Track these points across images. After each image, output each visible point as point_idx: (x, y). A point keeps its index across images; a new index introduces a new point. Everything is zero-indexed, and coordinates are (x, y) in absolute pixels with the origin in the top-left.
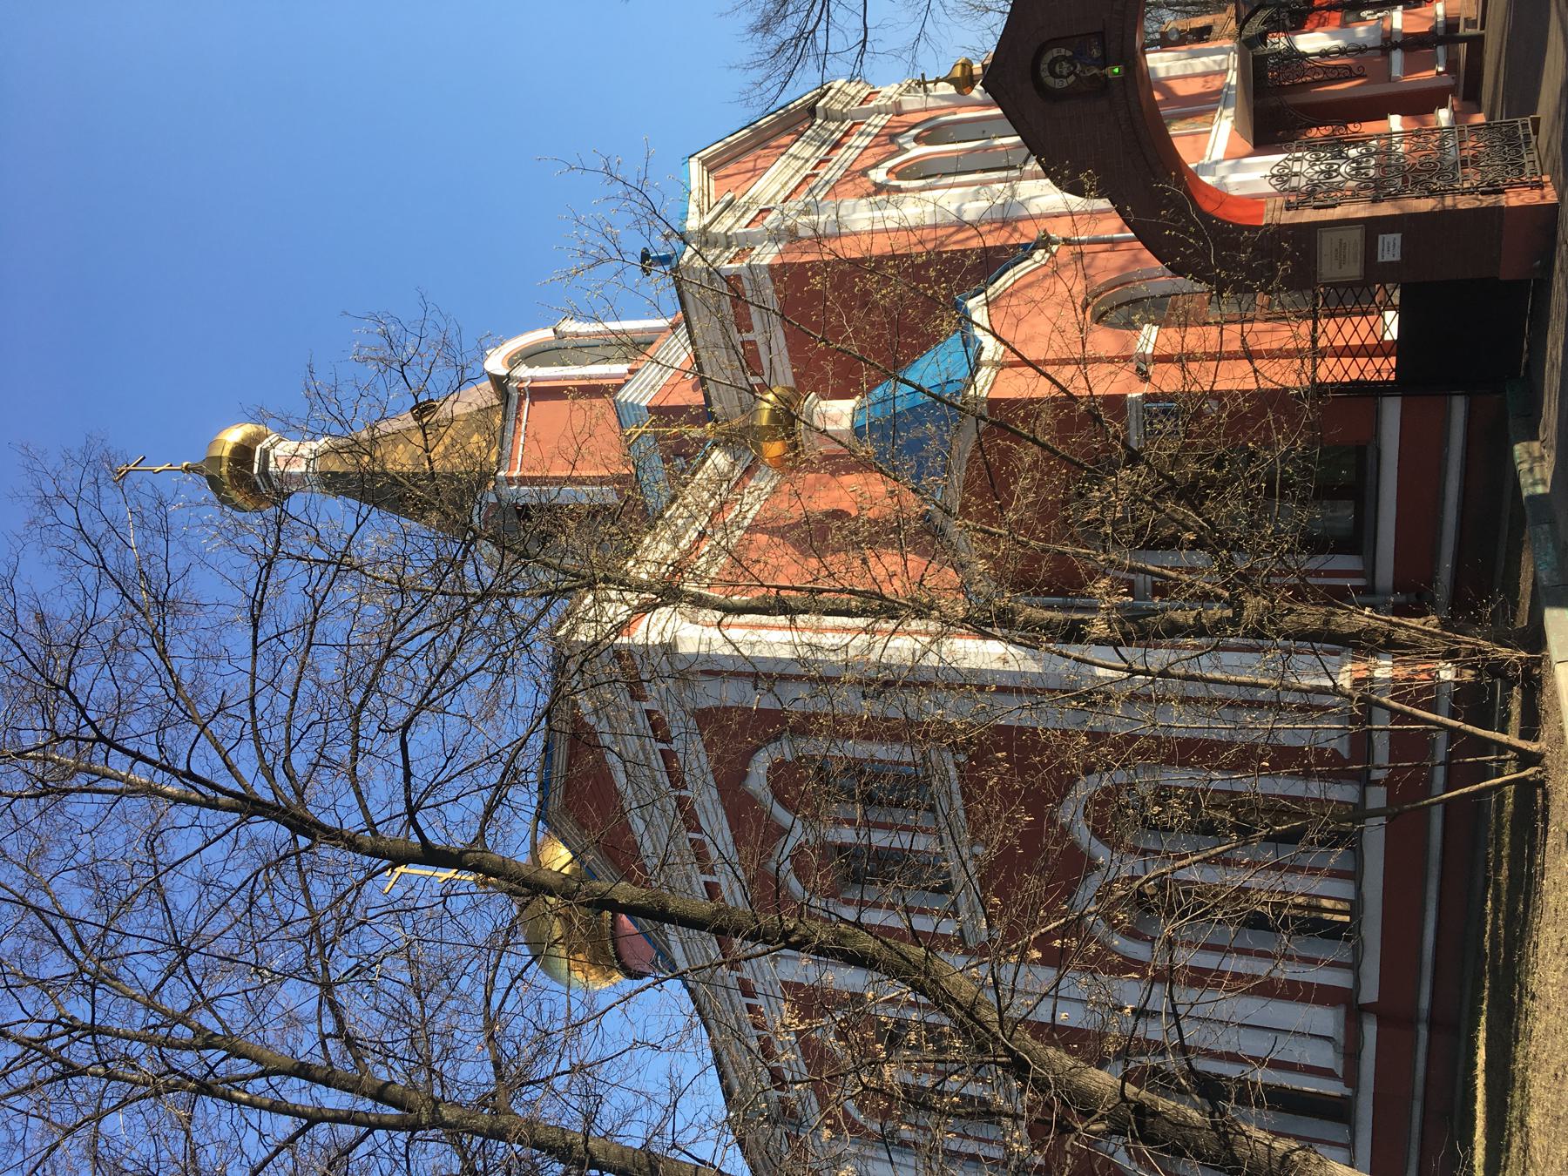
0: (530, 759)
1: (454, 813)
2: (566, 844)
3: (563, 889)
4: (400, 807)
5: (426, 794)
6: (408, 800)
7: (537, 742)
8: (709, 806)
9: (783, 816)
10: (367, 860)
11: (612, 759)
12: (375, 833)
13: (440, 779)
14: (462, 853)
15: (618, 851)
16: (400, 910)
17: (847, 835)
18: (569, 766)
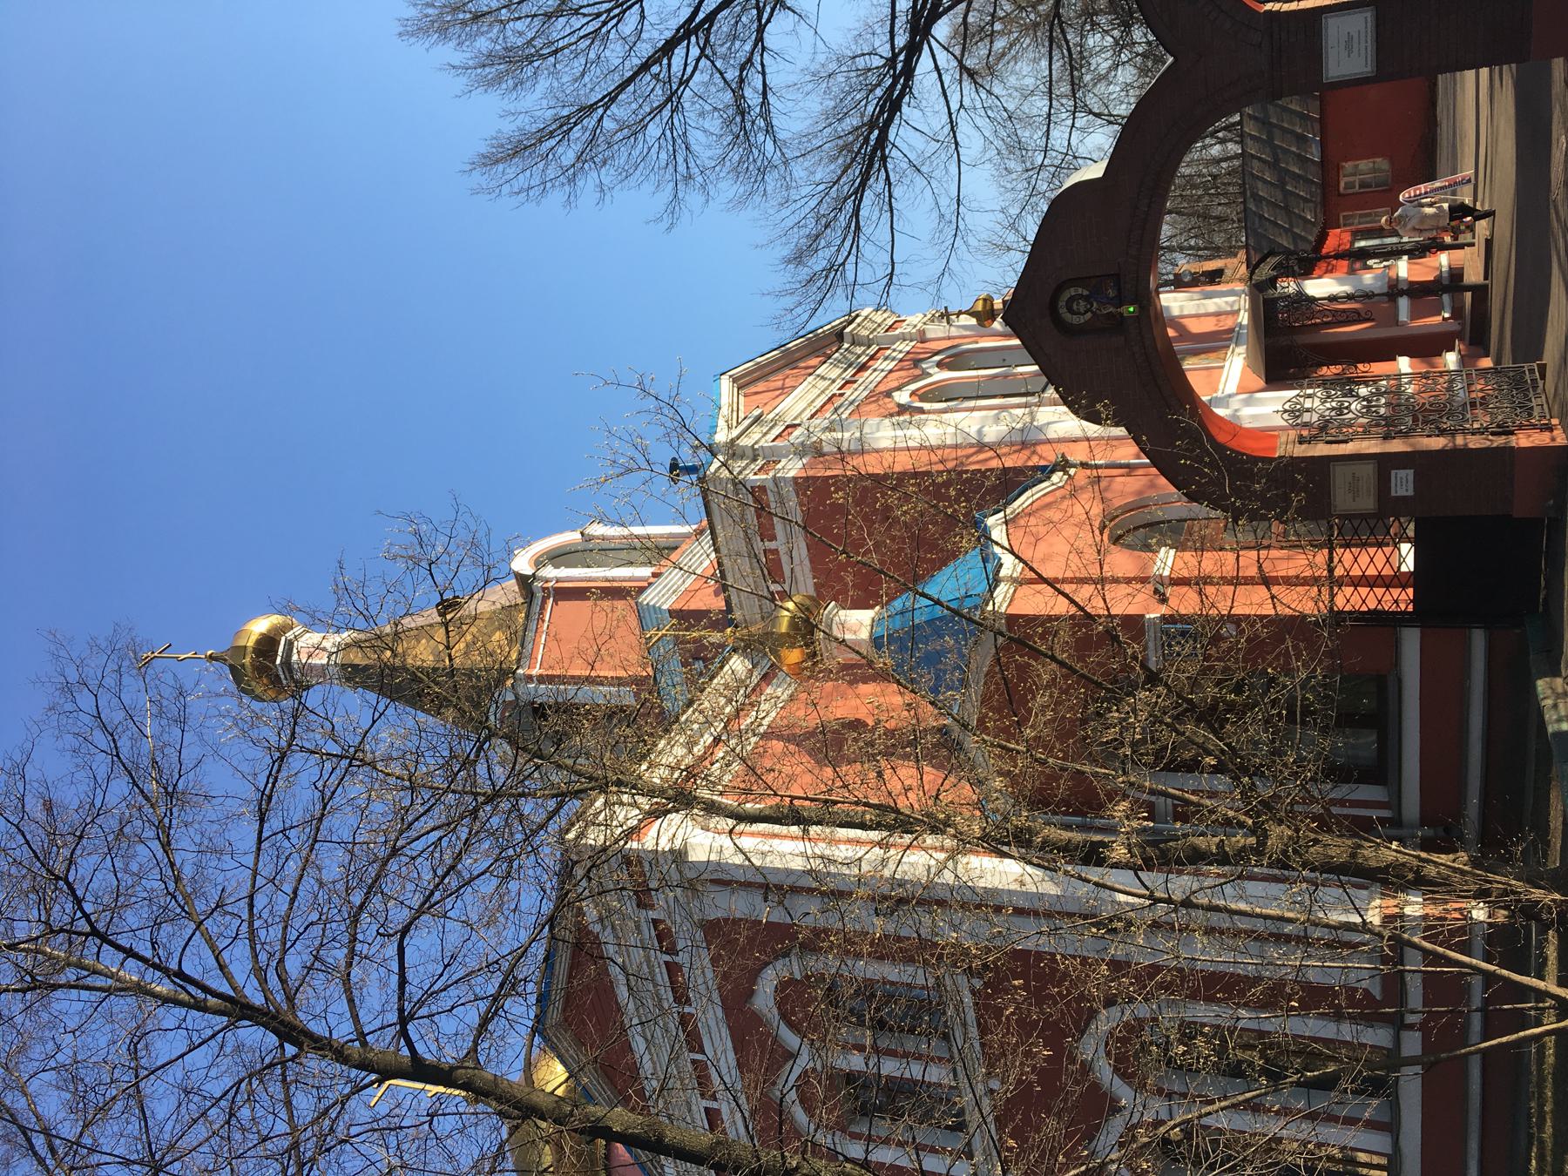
0: (530, 968)
1: (447, 1025)
2: (563, 1062)
3: (556, 1113)
4: (393, 1017)
5: (421, 1003)
6: (401, 1010)
7: (539, 950)
8: (712, 1023)
9: (791, 1039)
10: (354, 1072)
11: (614, 971)
12: (364, 1044)
13: (436, 987)
14: (452, 1069)
15: (612, 1068)
16: (385, 1128)
17: (856, 1062)
18: (570, 977)
